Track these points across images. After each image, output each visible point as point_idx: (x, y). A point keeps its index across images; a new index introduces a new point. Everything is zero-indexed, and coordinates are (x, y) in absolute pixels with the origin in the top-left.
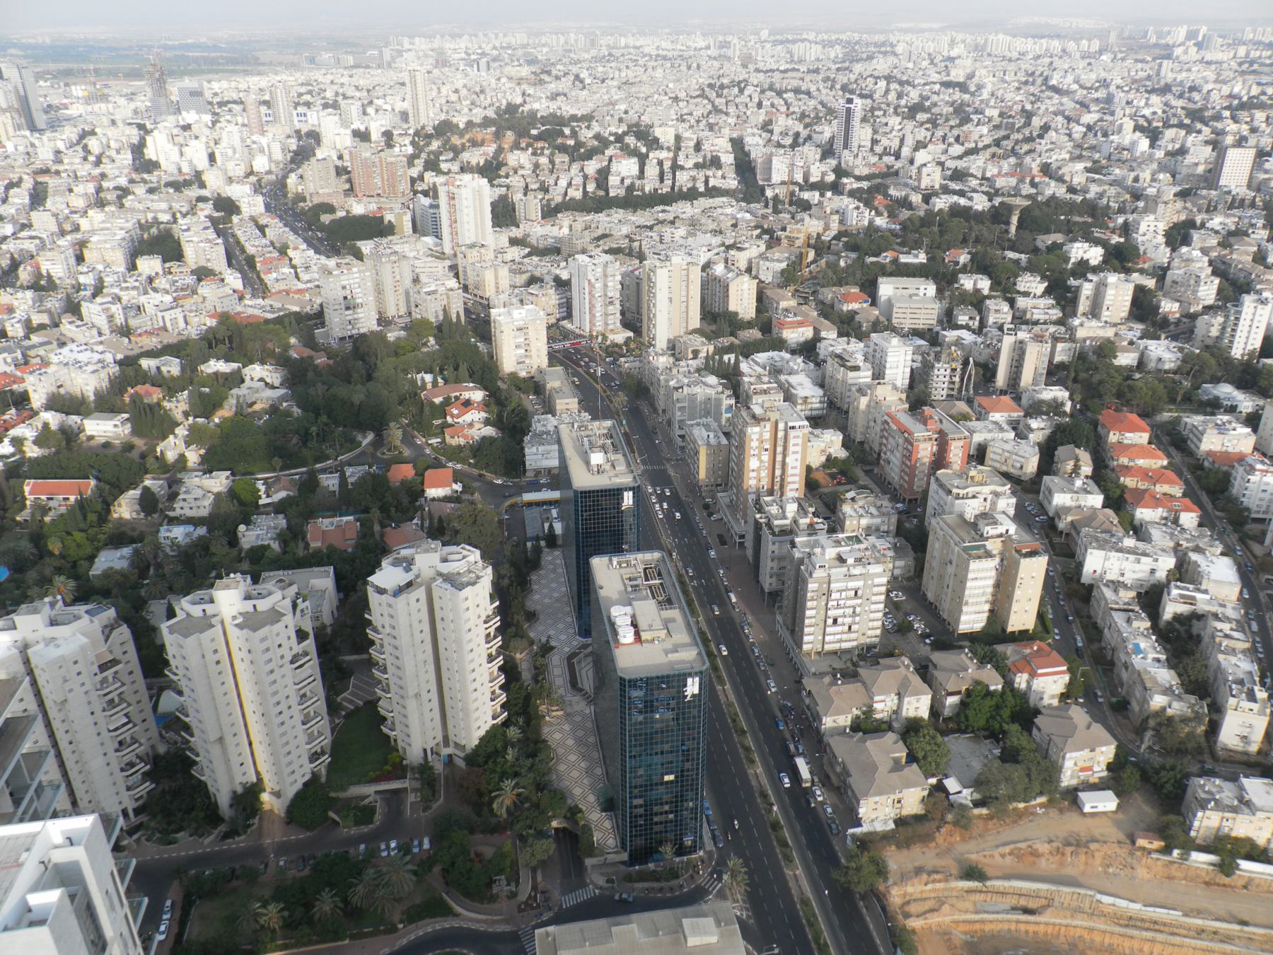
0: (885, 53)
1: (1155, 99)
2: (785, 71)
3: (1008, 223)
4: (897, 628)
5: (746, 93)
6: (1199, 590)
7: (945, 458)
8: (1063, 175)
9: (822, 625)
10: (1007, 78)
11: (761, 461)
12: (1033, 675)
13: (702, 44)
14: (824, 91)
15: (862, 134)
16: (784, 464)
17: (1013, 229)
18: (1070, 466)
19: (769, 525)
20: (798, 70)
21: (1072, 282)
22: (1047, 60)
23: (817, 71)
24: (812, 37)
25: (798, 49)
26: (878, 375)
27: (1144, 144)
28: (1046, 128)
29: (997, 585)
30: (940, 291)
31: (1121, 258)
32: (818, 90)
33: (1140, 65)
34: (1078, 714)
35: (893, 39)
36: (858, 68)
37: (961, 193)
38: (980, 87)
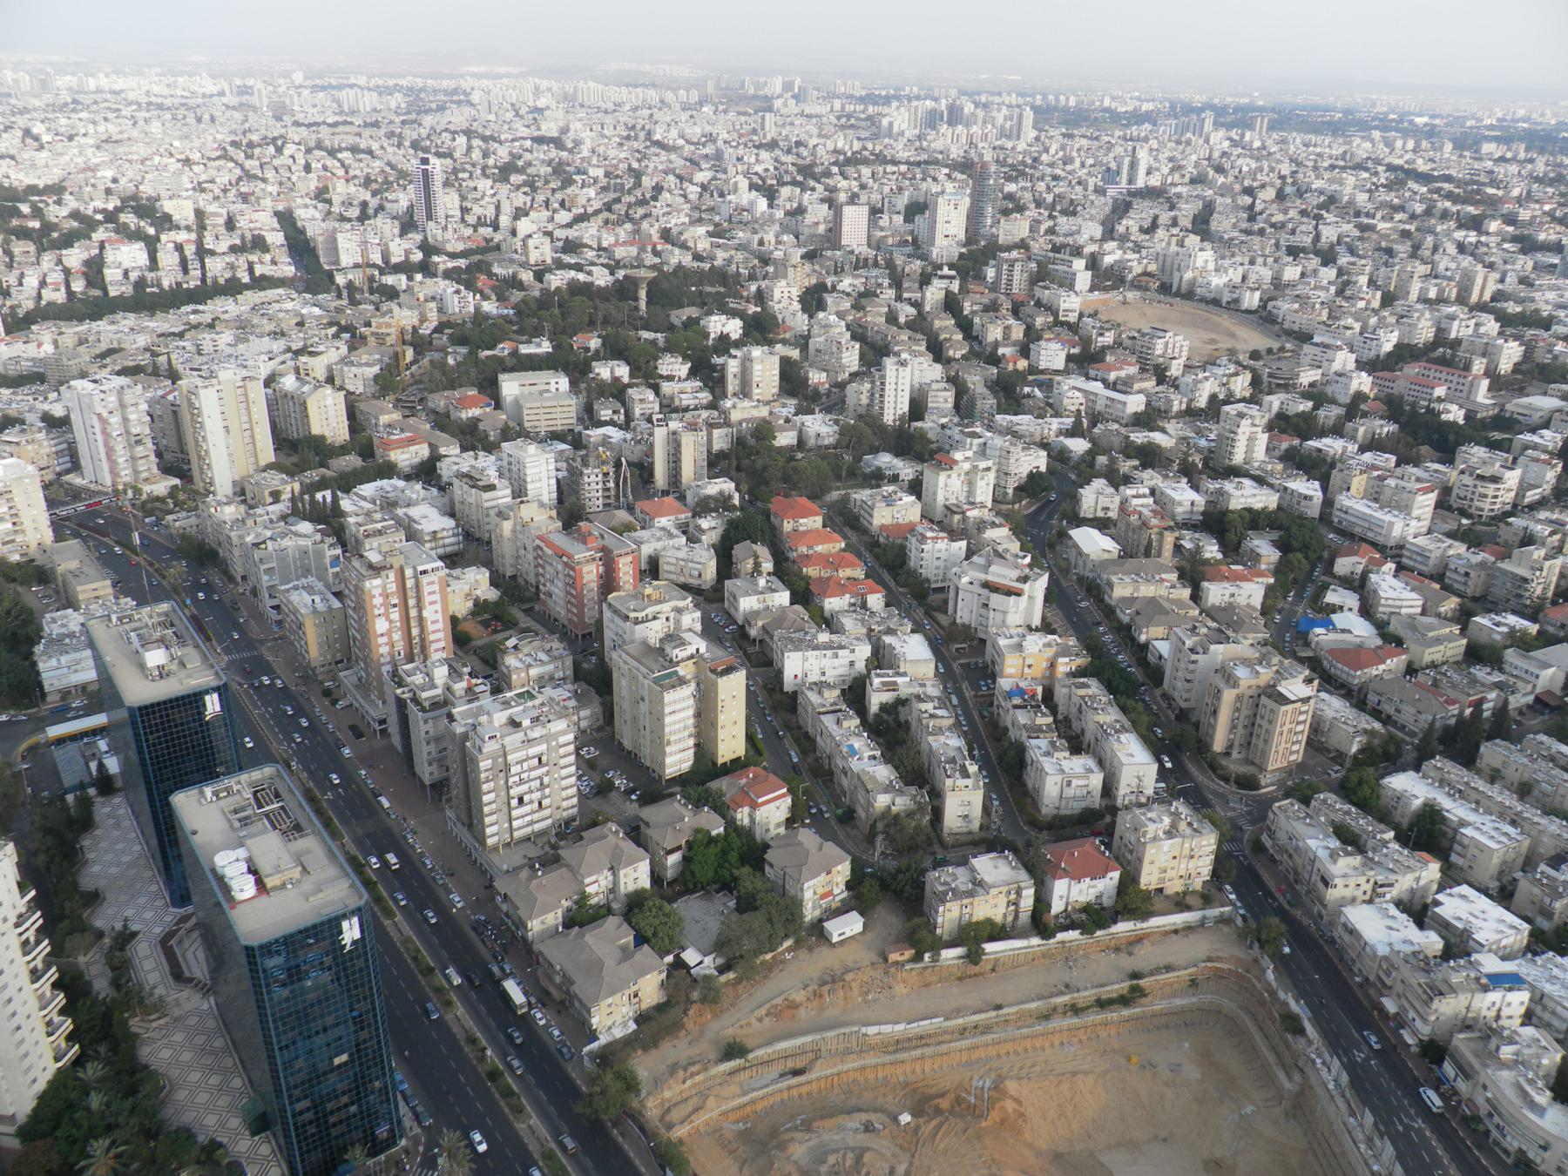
0: (459, 103)
2: (335, 125)
3: (636, 299)
5: (287, 152)
9: (505, 810)
12: (754, 806)
14: (390, 150)
15: (447, 202)
16: (421, 619)
19: (415, 700)
22: (646, 112)
24: (362, 81)
26: (519, 492)
27: (762, 204)
28: (658, 189)
30: (574, 384)
31: (761, 329)
32: (382, 148)
36: (428, 120)
37: (578, 267)
38: (577, 143)
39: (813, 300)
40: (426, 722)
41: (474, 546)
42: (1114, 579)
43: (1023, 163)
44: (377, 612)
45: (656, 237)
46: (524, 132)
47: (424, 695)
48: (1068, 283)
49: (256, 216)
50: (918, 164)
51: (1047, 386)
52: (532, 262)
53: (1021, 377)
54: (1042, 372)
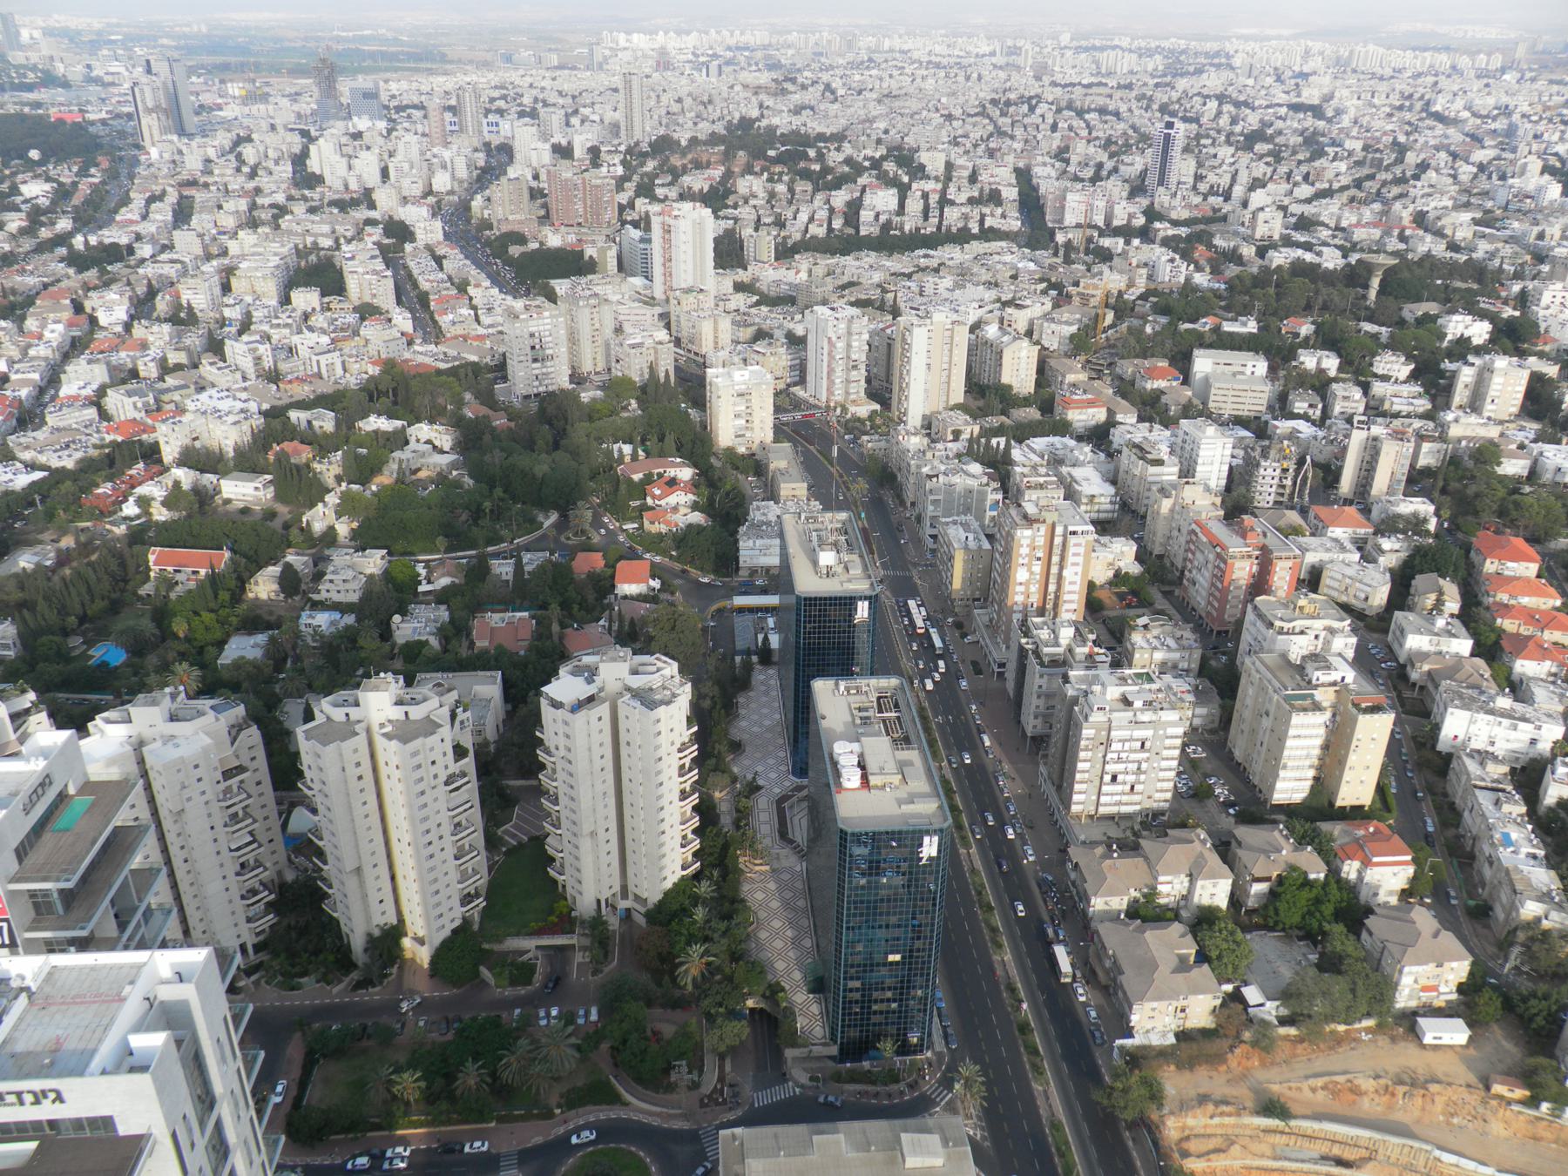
0: (1218, 66)
2: (1089, 86)
3: (1366, 287)
5: (1038, 111)
8: (1443, 227)
9: (1097, 783)
10: (1376, 101)
11: (1032, 573)
16: (1060, 577)
18: (1430, 600)
19: (1037, 653)
21: (1447, 365)
22: (1430, 79)
28: (1423, 167)
29: (1326, 747)
30: (1272, 370)
32: (1130, 110)
34: (1424, 918)
35: (1229, 48)
37: (1307, 247)
44: (1021, 561)
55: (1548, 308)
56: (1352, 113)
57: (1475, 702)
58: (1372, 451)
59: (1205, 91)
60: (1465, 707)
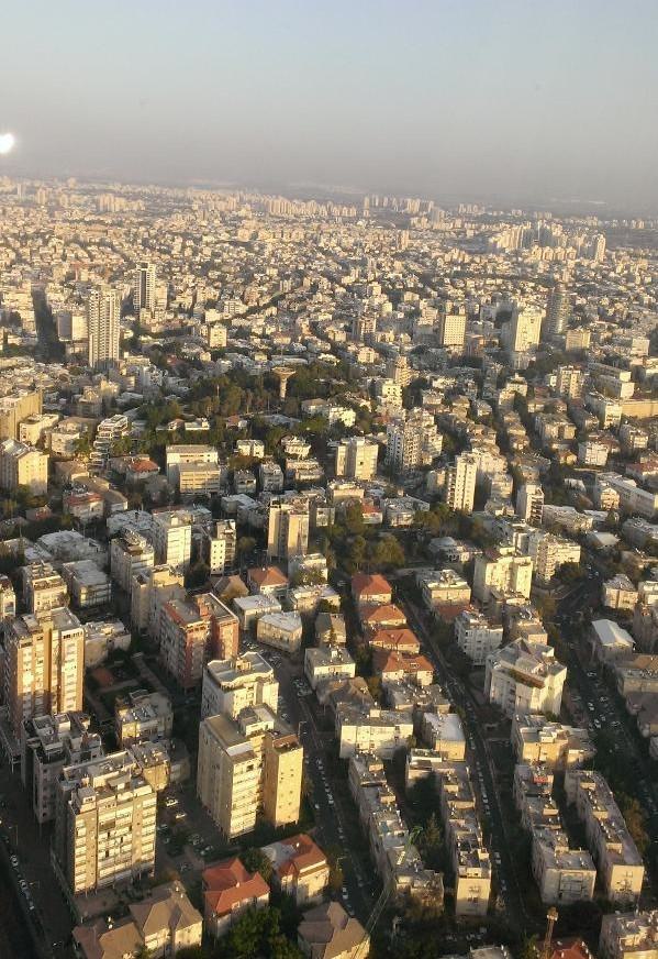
0: (183, 208)
1: (398, 264)
2: (90, 223)
3: (278, 390)
4: (171, 839)
5: (50, 244)
6: (432, 755)
7: (218, 637)
8: (327, 334)
9: (93, 862)
10: (284, 239)
11: (35, 674)
12: (297, 875)
13: (9, 188)
14: (126, 246)
15: (158, 292)
16: (59, 673)
17: (283, 395)
18: (327, 636)
19: (41, 750)
20: (102, 222)
21: (331, 443)
22: (316, 225)
23: (120, 224)
24: (117, 188)
25: (104, 200)
26: (161, 557)
27: (389, 307)
28: (315, 288)
29: (262, 782)
30: (222, 457)
31: (369, 424)
32: (121, 244)
33: (386, 232)
34: (336, 912)
35: (189, 194)
36: (159, 222)
37: (245, 352)
38: (262, 247)
39: (413, 395)
40: (45, 771)
41: (116, 603)
42: (625, 675)
43: (594, 279)
44: (25, 667)
45: (305, 330)
46: (224, 236)
47: (48, 748)
48: (614, 393)
49: (18, 296)
50: (511, 278)
51: (589, 478)
52: (212, 345)
53: (569, 471)
54: (587, 466)
55: (386, 396)
56: (270, 248)
57: (360, 719)
58: (284, 520)
59: (174, 230)
60: (352, 723)
